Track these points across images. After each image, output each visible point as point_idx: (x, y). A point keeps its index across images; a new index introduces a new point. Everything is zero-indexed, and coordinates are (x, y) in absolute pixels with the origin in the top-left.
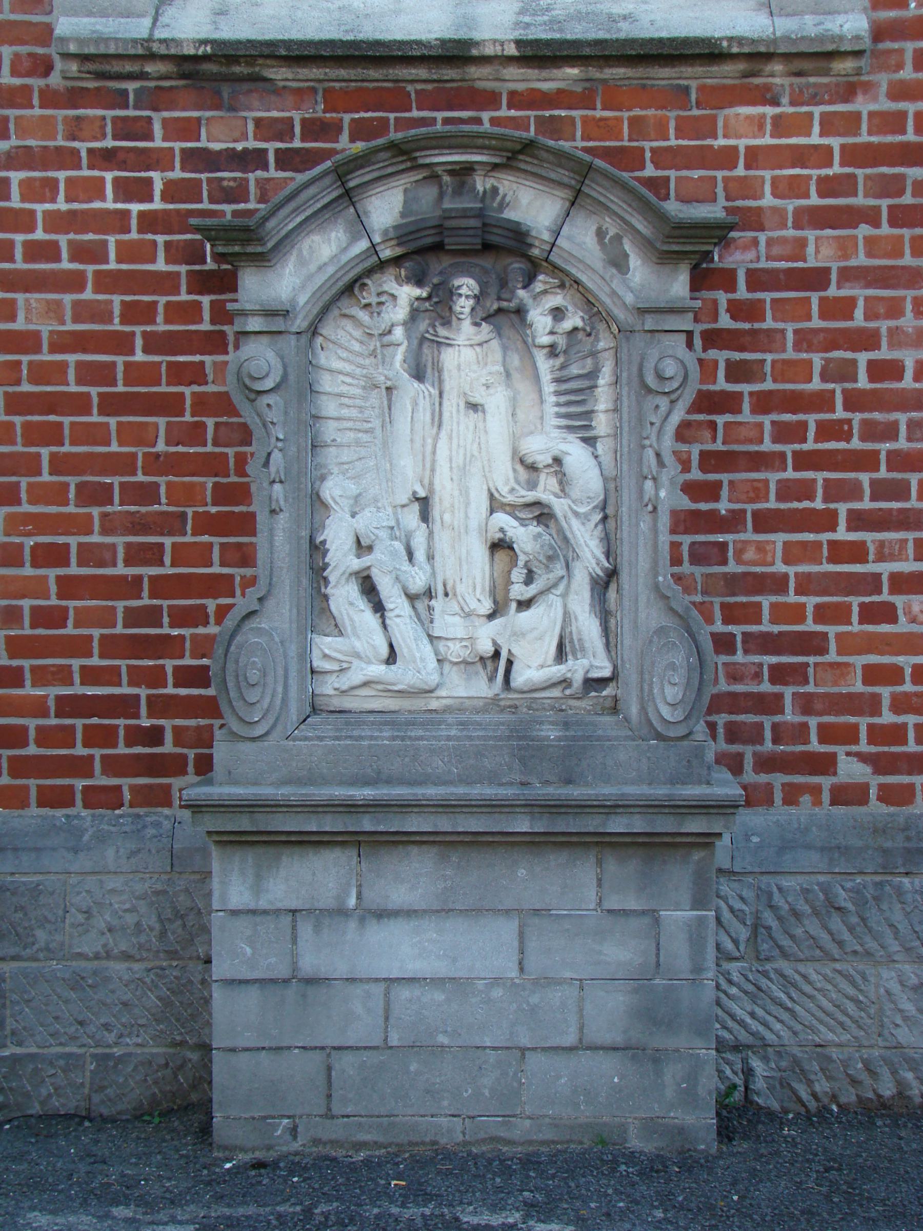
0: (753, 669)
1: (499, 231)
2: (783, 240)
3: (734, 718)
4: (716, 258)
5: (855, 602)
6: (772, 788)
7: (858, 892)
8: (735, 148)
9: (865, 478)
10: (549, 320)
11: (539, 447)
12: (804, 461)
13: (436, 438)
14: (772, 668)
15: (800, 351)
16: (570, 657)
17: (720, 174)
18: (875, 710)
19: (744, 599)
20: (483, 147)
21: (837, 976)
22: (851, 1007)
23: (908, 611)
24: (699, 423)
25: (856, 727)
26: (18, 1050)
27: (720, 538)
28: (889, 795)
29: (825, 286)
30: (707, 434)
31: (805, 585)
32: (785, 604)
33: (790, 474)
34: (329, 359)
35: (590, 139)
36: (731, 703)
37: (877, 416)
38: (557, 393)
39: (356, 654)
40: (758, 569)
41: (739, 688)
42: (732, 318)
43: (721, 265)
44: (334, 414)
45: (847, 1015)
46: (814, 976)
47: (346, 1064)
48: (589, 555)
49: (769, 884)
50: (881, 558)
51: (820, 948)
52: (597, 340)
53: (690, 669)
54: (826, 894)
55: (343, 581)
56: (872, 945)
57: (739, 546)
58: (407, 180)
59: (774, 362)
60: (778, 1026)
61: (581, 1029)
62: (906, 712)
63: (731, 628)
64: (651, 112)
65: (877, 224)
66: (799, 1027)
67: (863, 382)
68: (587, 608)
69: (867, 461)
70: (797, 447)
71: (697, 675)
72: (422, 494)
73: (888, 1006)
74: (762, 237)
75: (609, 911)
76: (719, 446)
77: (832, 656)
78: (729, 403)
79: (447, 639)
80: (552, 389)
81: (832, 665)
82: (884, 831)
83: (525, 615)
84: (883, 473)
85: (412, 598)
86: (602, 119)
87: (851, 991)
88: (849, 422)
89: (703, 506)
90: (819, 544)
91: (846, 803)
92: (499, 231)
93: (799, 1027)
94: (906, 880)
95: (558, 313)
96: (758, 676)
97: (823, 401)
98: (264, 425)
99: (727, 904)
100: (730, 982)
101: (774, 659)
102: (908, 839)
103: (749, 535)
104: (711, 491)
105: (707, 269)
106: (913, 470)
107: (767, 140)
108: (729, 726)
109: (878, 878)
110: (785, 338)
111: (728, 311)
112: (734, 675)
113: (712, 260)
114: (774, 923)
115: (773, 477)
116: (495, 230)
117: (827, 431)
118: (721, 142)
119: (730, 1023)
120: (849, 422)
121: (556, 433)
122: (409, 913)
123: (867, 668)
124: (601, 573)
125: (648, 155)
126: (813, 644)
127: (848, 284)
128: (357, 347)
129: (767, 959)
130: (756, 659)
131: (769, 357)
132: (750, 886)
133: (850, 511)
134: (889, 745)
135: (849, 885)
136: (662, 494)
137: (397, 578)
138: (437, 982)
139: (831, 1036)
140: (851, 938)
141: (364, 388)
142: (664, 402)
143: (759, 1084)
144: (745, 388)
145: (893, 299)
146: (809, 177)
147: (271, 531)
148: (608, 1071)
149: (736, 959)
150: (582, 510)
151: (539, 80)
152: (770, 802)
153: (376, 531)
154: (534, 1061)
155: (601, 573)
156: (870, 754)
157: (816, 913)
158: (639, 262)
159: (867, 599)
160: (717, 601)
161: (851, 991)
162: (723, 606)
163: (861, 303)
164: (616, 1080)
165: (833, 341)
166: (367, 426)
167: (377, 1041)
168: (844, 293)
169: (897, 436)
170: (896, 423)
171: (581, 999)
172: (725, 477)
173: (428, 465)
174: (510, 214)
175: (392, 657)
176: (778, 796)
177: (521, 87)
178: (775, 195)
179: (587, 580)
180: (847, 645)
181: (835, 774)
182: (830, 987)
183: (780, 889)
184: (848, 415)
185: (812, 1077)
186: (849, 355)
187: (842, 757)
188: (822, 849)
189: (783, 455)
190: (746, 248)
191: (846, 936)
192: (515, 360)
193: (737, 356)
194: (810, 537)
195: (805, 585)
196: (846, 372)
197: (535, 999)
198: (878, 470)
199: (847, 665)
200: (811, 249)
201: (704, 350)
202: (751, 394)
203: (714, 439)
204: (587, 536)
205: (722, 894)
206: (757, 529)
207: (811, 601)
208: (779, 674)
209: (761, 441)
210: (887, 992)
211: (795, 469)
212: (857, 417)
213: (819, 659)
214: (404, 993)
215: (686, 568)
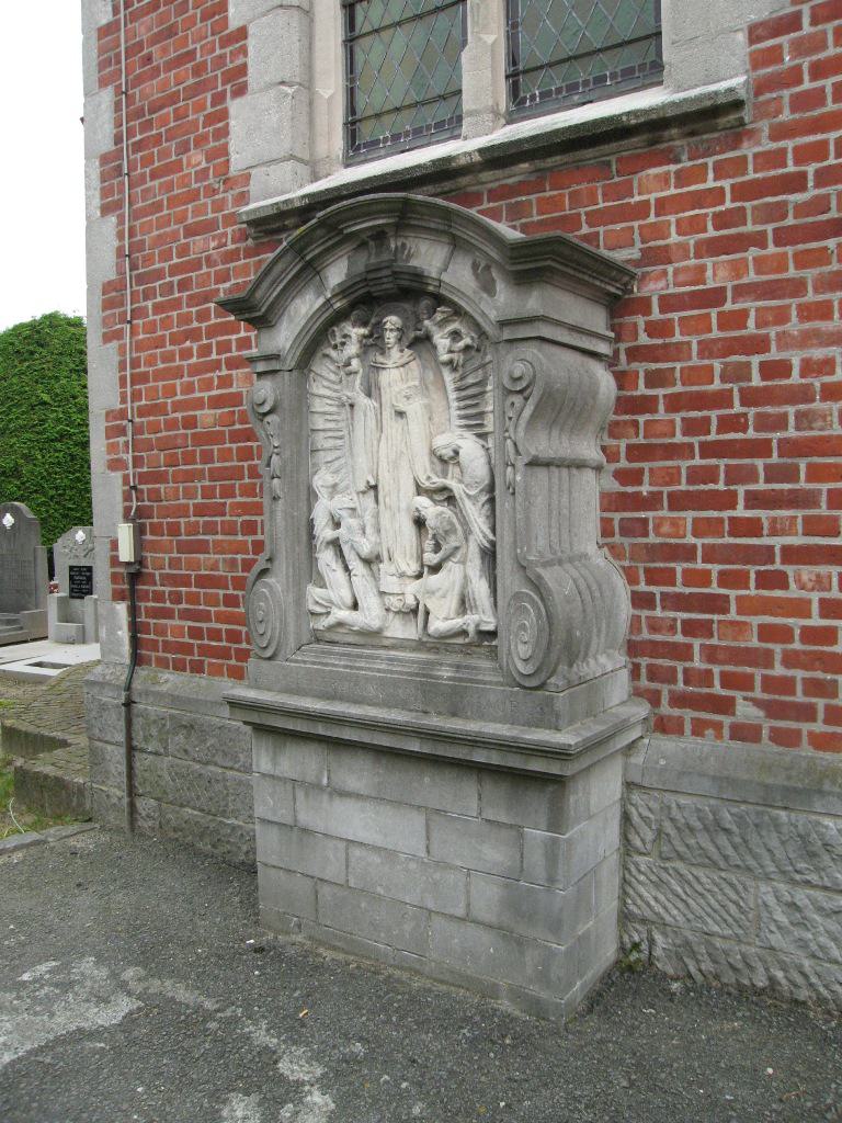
0: (669, 623)
1: (406, 277)
2: (686, 269)
3: (654, 661)
4: (635, 290)
5: (752, 570)
6: (683, 721)
7: (741, 817)
8: (648, 201)
9: (759, 463)
10: (447, 342)
11: (444, 442)
12: (709, 450)
13: (379, 441)
14: (684, 622)
15: (703, 358)
16: (469, 612)
17: (636, 224)
18: (769, 664)
19: (662, 565)
20: (382, 212)
21: (722, 881)
22: (733, 909)
23: (798, 580)
24: (625, 422)
25: (751, 677)
26: (236, 822)
27: (643, 515)
28: (779, 737)
29: (723, 301)
30: (632, 431)
31: (711, 555)
32: (695, 570)
33: (697, 461)
34: (318, 388)
35: (543, 214)
36: (655, 649)
37: (769, 409)
38: (459, 399)
39: (343, 596)
40: (672, 541)
41: (658, 637)
42: (648, 336)
43: (639, 295)
44: (321, 427)
45: (730, 915)
46: (704, 880)
47: (326, 890)
48: (477, 530)
49: (670, 801)
50: (774, 532)
51: (709, 858)
52: (485, 354)
53: (540, 631)
54: (714, 815)
55: (323, 547)
56: (751, 862)
57: (657, 521)
58: (348, 249)
59: (682, 369)
60: (675, 912)
61: (468, 905)
62: (794, 666)
63: (652, 589)
64: (584, 186)
65: (763, 246)
66: (690, 916)
67: (756, 381)
68: (478, 573)
69: (762, 449)
70: (703, 438)
71: (545, 635)
72: (373, 483)
73: (765, 914)
74: (670, 269)
75: (488, 821)
76: (641, 440)
77: (733, 615)
78: (647, 405)
79: (390, 594)
80: (455, 397)
81: (732, 623)
82: (770, 768)
83: (434, 578)
84: (775, 459)
85: (367, 562)
86: (551, 197)
87: (734, 897)
88: (745, 415)
89: (630, 489)
90: (720, 520)
91: (743, 739)
92: (406, 277)
93: (690, 916)
94: (783, 814)
95: (456, 335)
96: (672, 629)
97: (723, 399)
98: (267, 435)
99: (637, 810)
100: (639, 871)
101: (686, 616)
102: (789, 778)
103: (665, 513)
104: (633, 477)
105: (629, 299)
106: (800, 456)
107: (673, 191)
108: (650, 668)
109: (760, 808)
110: (690, 349)
111: (645, 331)
112: (654, 626)
113: (632, 291)
114: (673, 832)
115: (684, 464)
116: (402, 276)
117: (727, 424)
118: (637, 198)
119: (639, 902)
120: (745, 415)
121: (459, 431)
122: (358, 796)
123: (761, 627)
124: (487, 545)
125: (583, 218)
126: (717, 604)
127: (742, 299)
128: (332, 377)
129: (668, 859)
130: (672, 614)
131: (678, 365)
132: (656, 799)
133: (747, 492)
134: (780, 694)
135: (734, 810)
136: (518, 478)
137: (352, 546)
138: (376, 849)
139: (716, 928)
140: (735, 854)
141: (338, 406)
142: (518, 400)
143: (658, 952)
144: (660, 392)
145: (779, 307)
146: (706, 215)
147: (272, 512)
148: (486, 943)
149: (645, 854)
150: (472, 493)
151: (505, 178)
152: (681, 732)
153: (340, 512)
154: (437, 921)
155: (487, 545)
156: (764, 701)
157: (706, 828)
158: (503, 286)
159: (763, 568)
160: (641, 566)
161: (734, 897)
162: (647, 571)
163: (752, 314)
164: (492, 950)
165: (730, 347)
166: (341, 434)
167: (341, 881)
168: (737, 306)
169: (787, 425)
170: (785, 415)
171: (467, 885)
172: (646, 465)
173: (375, 460)
174: (414, 263)
175: (355, 606)
176: (688, 728)
177: (494, 185)
178: (679, 233)
179: (477, 550)
180: (746, 606)
181: (733, 714)
182: (716, 890)
183: (678, 806)
184: (744, 410)
185: (700, 958)
186: (743, 358)
187: (739, 701)
188: (714, 778)
189: (691, 446)
190: (657, 279)
191: (730, 851)
192: (430, 376)
193: (653, 366)
194: (715, 514)
195: (711, 555)
196: (741, 373)
197: (437, 876)
198: (770, 456)
199: (745, 623)
200: (709, 273)
201: (628, 364)
202: (665, 396)
203: (637, 435)
204: (476, 514)
205: (634, 802)
206: (671, 508)
207: (715, 568)
208: (690, 628)
209: (674, 435)
210: (764, 903)
211: (701, 457)
212: (752, 412)
213: (722, 617)
214: (357, 852)
215: (617, 539)
